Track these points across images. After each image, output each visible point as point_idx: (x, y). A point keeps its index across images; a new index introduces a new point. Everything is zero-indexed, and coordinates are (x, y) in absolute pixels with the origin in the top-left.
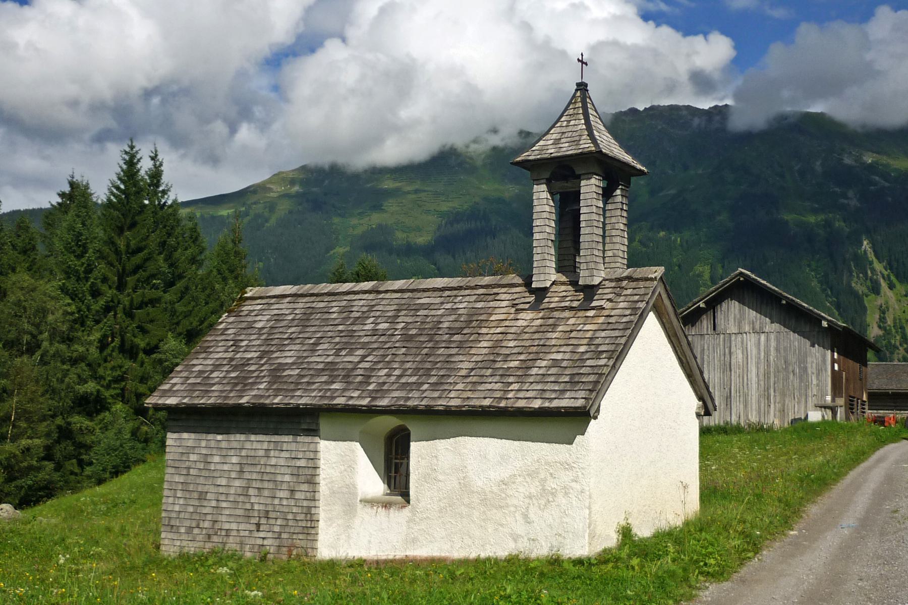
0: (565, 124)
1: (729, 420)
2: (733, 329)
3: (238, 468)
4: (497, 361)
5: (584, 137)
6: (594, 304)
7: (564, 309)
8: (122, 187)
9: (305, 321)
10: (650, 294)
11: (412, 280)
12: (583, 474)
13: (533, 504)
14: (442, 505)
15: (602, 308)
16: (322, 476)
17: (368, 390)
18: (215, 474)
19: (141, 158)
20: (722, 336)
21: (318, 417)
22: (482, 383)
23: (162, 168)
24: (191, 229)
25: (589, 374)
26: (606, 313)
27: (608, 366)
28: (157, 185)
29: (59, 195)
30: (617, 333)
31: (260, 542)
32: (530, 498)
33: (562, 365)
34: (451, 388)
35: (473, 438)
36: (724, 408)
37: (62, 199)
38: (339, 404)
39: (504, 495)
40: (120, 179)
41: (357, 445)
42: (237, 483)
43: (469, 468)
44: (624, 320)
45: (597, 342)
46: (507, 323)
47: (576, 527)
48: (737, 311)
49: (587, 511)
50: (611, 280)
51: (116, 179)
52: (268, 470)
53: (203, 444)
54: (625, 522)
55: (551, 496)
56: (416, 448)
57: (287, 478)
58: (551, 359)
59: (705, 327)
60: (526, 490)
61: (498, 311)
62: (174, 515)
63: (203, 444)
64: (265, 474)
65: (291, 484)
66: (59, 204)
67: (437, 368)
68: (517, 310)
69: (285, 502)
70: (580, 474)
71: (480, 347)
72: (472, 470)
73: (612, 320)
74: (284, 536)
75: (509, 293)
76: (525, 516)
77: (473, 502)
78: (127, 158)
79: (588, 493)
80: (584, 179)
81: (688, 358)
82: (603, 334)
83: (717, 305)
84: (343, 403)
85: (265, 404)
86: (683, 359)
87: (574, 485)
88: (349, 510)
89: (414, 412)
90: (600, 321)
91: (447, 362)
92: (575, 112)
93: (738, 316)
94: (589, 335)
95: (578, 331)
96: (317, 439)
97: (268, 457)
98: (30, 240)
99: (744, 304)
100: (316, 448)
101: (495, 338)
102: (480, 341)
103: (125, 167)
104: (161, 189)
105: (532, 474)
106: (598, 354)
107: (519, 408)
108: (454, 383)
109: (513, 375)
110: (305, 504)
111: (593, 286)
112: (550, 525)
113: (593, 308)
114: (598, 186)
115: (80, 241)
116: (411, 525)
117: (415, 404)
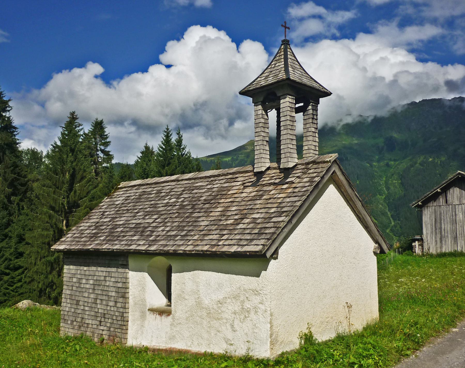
0: (273, 66)
1: (456, 249)
2: (456, 202)
3: (92, 287)
4: (222, 220)
5: (282, 72)
6: (289, 180)
7: (270, 184)
8: (164, 147)
9: (139, 199)
10: (325, 171)
11: (197, 173)
12: (266, 298)
13: (237, 318)
14: (187, 316)
15: (292, 183)
16: (130, 294)
17: (149, 240)
18: (84, 290)
19: (172, 134)
20: (451, 206)
21: (127, 257)
22: (209, 235)
23: (182, 138)
24: (197, 165)
25: (271, 227)
26: (294, 185)
27: (284, 221)
28: (180, 146)
29: (141, 152)
30: (296, 199)
31: (101, 332)
32: (235, 313)
33: (257, 222)
34: (191, 238)
35: (203, 272)
36: (453, 243)
37: (142, 154)
38: (132, 249)
39: (220, 311)
40: (163, 144)
41: (146, 275)
42: (92, 296)
43: (201, 292)
44: (304, 189)
45: (283, 205)
46: (236, 196)
47: (262, 337)
48: (458, 193)
49: (269, 326)
50: (302, 164)
51: (161, 144)
52: (106, 288)
53: (79, 272)
54: (308, 330)
55: (247, 313)
56: (175, 277)
57: (113, 294)
58: (252, 218)
59: (441, 201)
60: (233, 308)
61: (235, 188)
62: (66, 313)
63: (79, 272)
64: (104, 291)
65: (115, 297)
66: (141, 156)
67: (189, 225)
68: (244, 187)
69: (112, 309)
70: (264, 298)
71: (217, 212)
72: (202, 293)
73: (296, 190)
74: (112, 329)
75: (244, 177)
76: (232, 326)
77: (203, 315)
78: (166, 134)
79: (269, 312)
80: (282, 99)
81: (363, 216)
82: (288, 200)
83: (447, 190)
84: (134, 248)
85: (89, 249)
86: (360, 216)
87: (260, 306)
88: (143, 316)
89: (175, 255)
90: (289, 191)
91: (196, 221)
92: (280, 58)
93: (459, 195)
94: (279, 201)
95: (274, 198)
96: (127, 270)
97: (106, 281)
98: (124, 172)
99: (462, 189)
100: (127, 276)
101: (226, 205)
102: (218, 207)
103: (165, 138)
104: (182, 147)
105: (236, 297)
106: (280, 214)
107: (223, 252)
108: (194, 235)
109: (227, 229)
110: (121, 310)
111: (289, 168)
112: (247, 334)
113: (287, 183)
114: (292, 103)
115: (146, 172)
116: (173, 328)
117: (168, 249)
